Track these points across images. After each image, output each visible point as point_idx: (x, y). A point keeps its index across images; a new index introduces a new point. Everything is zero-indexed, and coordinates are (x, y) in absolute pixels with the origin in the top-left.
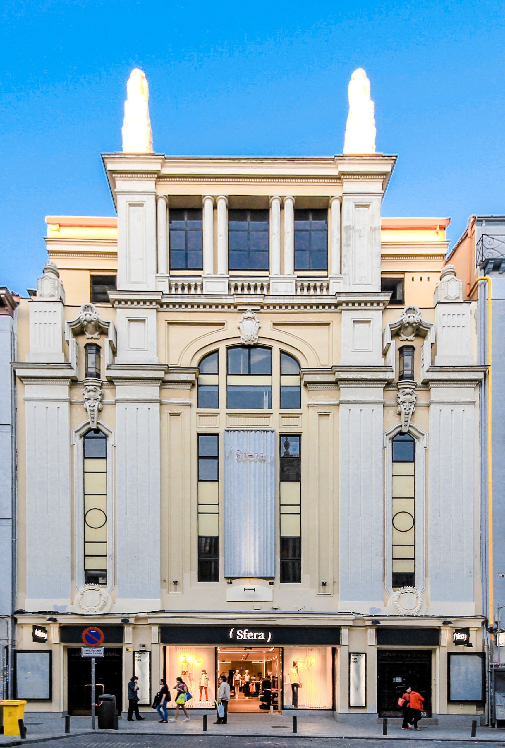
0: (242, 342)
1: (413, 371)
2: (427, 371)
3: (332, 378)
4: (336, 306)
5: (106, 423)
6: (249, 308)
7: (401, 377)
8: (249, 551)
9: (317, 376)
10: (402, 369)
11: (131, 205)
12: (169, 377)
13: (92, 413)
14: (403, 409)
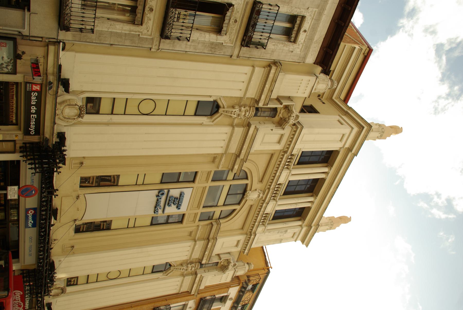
0: (247, 192)
1: (260, 116)
3: (211, 236)
4: (251, 232)
6: (264, 197)
8: (99, 205)
9: (214, 231)
10: (263, 110)
11: (343, 135)
12: (238, 160)
13: (230, 112)
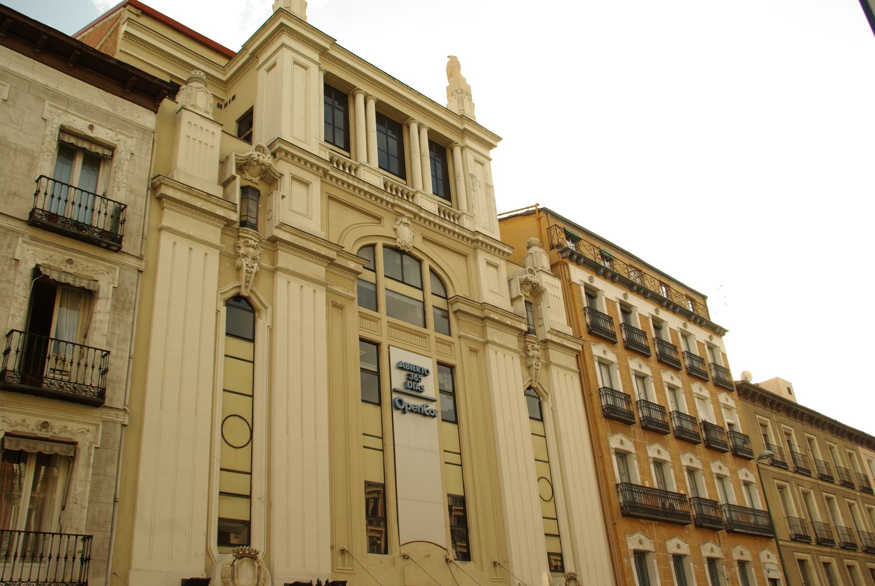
2: (276, 227)
3: (478, 313)
4: (472, 241)
5: (260, 295)
7: (243, 224)
10: (245, 213)
12: (340, 261)
13: (249, 275)
14: (244, 263)
